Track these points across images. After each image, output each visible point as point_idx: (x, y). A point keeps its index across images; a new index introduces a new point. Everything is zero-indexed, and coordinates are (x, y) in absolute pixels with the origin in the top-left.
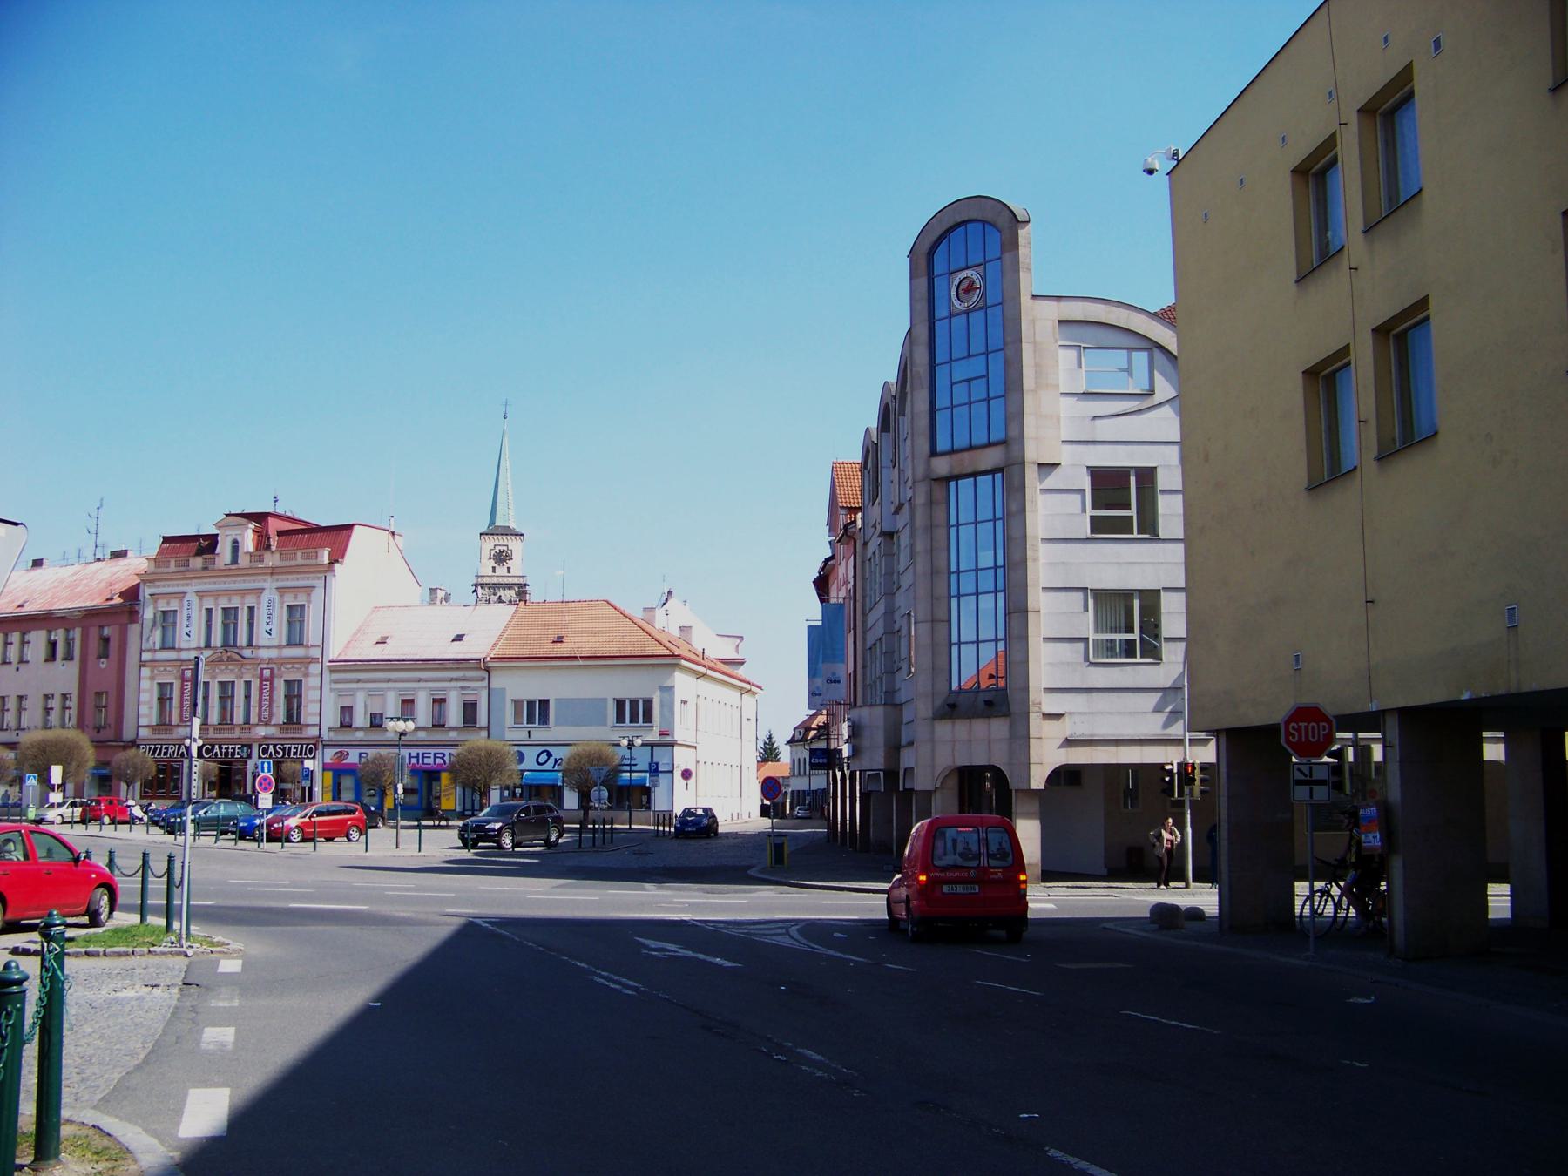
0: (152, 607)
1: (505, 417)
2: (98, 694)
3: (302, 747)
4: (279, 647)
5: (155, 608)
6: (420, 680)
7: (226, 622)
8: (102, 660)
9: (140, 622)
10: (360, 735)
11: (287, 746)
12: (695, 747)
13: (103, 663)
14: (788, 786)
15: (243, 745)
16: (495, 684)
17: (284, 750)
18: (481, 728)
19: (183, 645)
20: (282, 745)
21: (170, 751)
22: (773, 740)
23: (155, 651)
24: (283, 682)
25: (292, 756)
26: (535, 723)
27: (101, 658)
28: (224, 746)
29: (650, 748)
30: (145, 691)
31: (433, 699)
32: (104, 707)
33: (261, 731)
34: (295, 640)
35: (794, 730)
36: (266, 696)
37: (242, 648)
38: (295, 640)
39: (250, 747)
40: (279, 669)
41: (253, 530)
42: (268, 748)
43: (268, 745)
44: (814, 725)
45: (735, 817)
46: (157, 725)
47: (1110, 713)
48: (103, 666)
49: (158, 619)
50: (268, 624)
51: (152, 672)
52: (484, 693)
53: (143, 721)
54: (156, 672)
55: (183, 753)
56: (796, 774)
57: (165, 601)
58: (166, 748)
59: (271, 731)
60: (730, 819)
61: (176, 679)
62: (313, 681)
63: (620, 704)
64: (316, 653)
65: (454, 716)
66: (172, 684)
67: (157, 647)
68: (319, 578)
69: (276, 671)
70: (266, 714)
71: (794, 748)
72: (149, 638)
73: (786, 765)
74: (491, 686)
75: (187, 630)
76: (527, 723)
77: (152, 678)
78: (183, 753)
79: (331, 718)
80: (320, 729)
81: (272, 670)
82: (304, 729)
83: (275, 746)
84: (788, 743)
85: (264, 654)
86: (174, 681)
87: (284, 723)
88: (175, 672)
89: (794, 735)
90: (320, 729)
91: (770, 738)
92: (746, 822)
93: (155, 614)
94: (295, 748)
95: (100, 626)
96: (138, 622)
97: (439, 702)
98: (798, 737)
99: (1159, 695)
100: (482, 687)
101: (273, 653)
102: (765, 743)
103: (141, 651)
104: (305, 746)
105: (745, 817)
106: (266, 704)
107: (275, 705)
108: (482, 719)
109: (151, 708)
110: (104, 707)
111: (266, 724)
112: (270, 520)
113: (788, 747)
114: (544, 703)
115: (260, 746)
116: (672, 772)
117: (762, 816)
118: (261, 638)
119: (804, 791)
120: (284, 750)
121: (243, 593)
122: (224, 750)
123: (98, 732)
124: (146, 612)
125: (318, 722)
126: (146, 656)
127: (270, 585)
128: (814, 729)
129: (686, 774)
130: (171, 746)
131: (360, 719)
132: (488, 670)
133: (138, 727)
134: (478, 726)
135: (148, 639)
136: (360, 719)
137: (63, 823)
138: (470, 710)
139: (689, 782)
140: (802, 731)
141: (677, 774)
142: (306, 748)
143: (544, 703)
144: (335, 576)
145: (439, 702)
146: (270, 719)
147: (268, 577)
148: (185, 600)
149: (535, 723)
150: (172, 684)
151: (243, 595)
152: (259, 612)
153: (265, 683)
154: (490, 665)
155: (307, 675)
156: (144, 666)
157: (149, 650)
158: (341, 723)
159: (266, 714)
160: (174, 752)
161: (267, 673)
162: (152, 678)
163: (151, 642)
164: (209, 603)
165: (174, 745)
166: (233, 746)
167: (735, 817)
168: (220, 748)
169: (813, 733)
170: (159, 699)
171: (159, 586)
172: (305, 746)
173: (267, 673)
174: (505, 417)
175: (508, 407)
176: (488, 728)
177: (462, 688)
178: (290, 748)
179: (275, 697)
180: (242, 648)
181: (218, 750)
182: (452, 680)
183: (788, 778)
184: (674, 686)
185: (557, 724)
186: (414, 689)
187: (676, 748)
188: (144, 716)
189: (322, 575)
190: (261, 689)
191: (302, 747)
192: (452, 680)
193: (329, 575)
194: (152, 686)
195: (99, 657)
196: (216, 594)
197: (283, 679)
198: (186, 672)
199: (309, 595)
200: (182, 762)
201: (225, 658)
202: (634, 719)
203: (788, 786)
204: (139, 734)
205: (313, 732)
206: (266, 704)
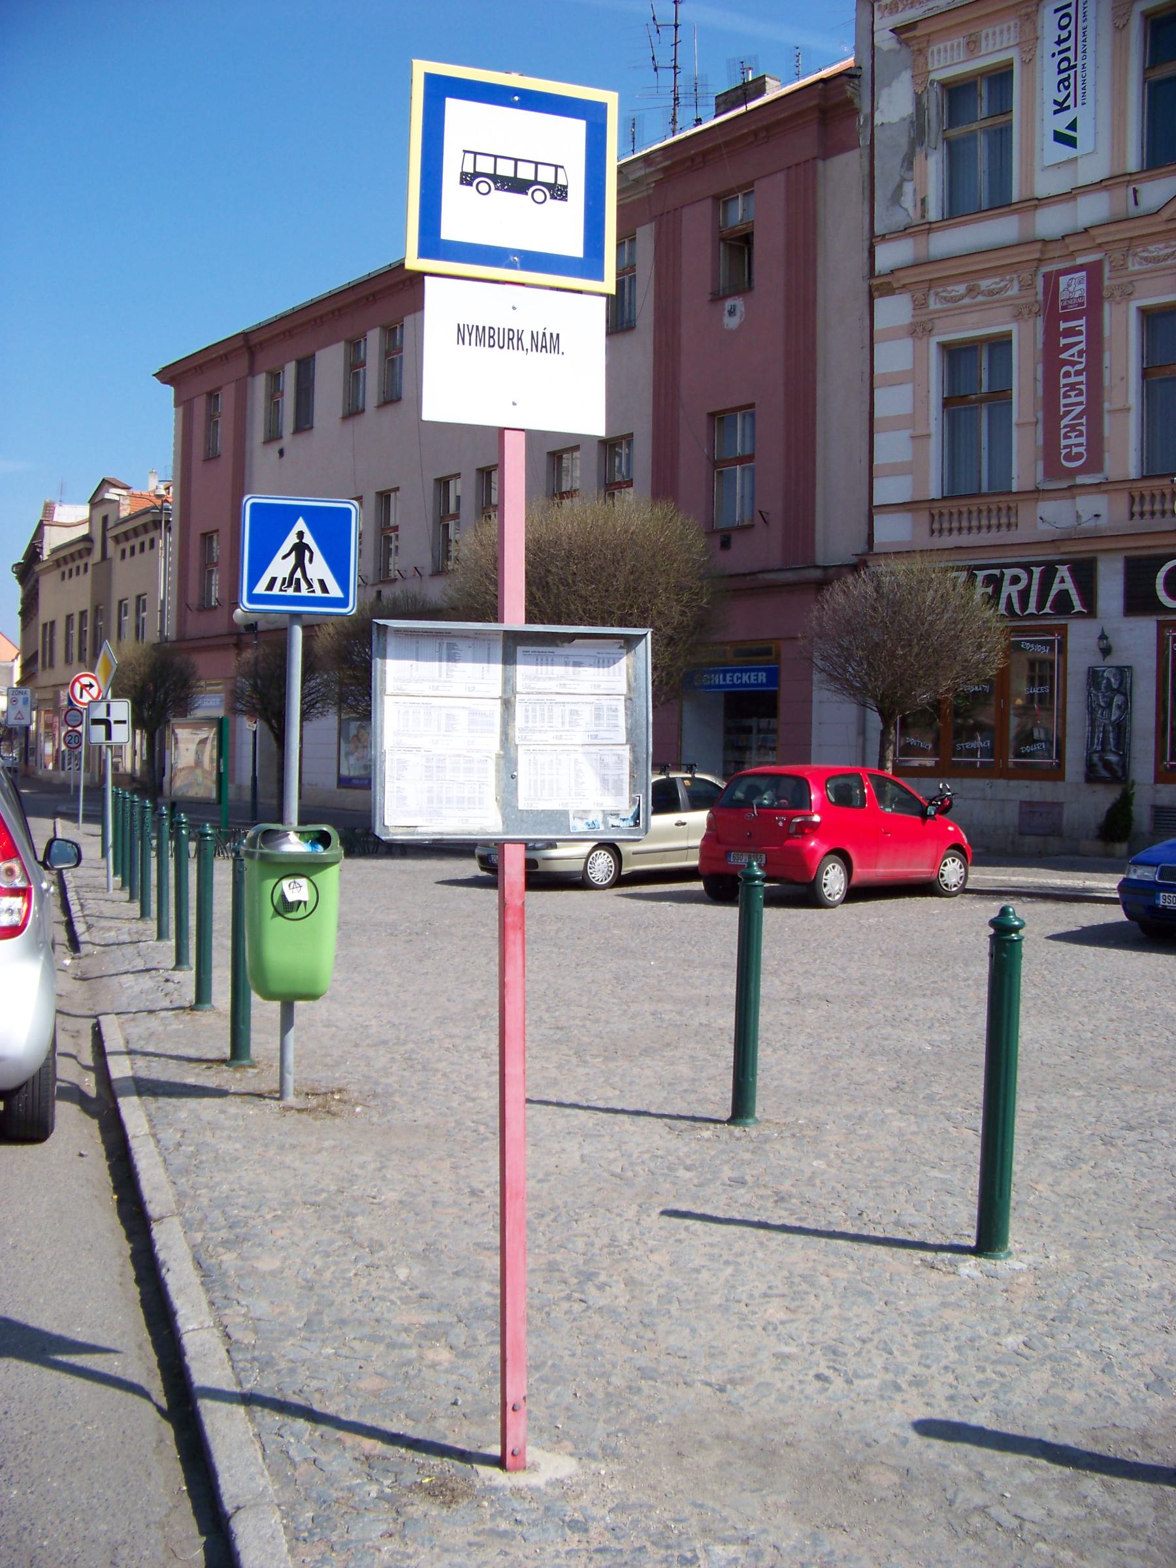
0: (906, 76)
2: (719, 419)
5: (920, 75)
7: (954, 133)
8: (728, 303)
9: (864, 141)
13: (732, 313)
19: (1044, 186)
23: (928, 228)
24: (934, 350)
27: (725, 297)
30: (895, 380)
32: (741, 460)
35: (76, 845)
36: (1073, 377)
46: (944, 498)
48: (732, 323)
49: (933, 112)
50: (1061, 107)
51: (919, 305)
53: (887, 491)
54: (934, 304)
55: (1064, 594)
57: (959, 40)
58: (989, 580)
61: (1017, 317)
66: (1000, 344)
67: (933, 214)
69: (1108, 280)
70: (1076, 443)
72: (900, 187)
75: (1061, 123)
77: (919, 330)
78: (1064, 594)
88: (1014, 290)
93: (918, 100)
95: (716, 198)
96: (853, 146)
99: (30, 820)
103: (873, 240)
106: (1073, 403)
109: (919, 439)
110: (741, 460)
123: (726, 544)
124: (882, 102)
126: (889, 256)
130: (1009, 573)
133: (872, 511)
135: (896, 196)
137: (621, 880)
150: (1000, 344)
156: (888, 290)
157: (906, 231)
159: (1076, 443)
160: (1024, 595)
161: (1073, 287)
162: (919, 330)
163: (908, 201)
165: (1027, 567)
170: (947, 403)
173: (1073, 287)
188: (896, 470)
195: (717, 297)
197: (1134, 305)
198: (1063, 281)
200: (1063, 629)
204: (877, 539)
206: (1073, 403)
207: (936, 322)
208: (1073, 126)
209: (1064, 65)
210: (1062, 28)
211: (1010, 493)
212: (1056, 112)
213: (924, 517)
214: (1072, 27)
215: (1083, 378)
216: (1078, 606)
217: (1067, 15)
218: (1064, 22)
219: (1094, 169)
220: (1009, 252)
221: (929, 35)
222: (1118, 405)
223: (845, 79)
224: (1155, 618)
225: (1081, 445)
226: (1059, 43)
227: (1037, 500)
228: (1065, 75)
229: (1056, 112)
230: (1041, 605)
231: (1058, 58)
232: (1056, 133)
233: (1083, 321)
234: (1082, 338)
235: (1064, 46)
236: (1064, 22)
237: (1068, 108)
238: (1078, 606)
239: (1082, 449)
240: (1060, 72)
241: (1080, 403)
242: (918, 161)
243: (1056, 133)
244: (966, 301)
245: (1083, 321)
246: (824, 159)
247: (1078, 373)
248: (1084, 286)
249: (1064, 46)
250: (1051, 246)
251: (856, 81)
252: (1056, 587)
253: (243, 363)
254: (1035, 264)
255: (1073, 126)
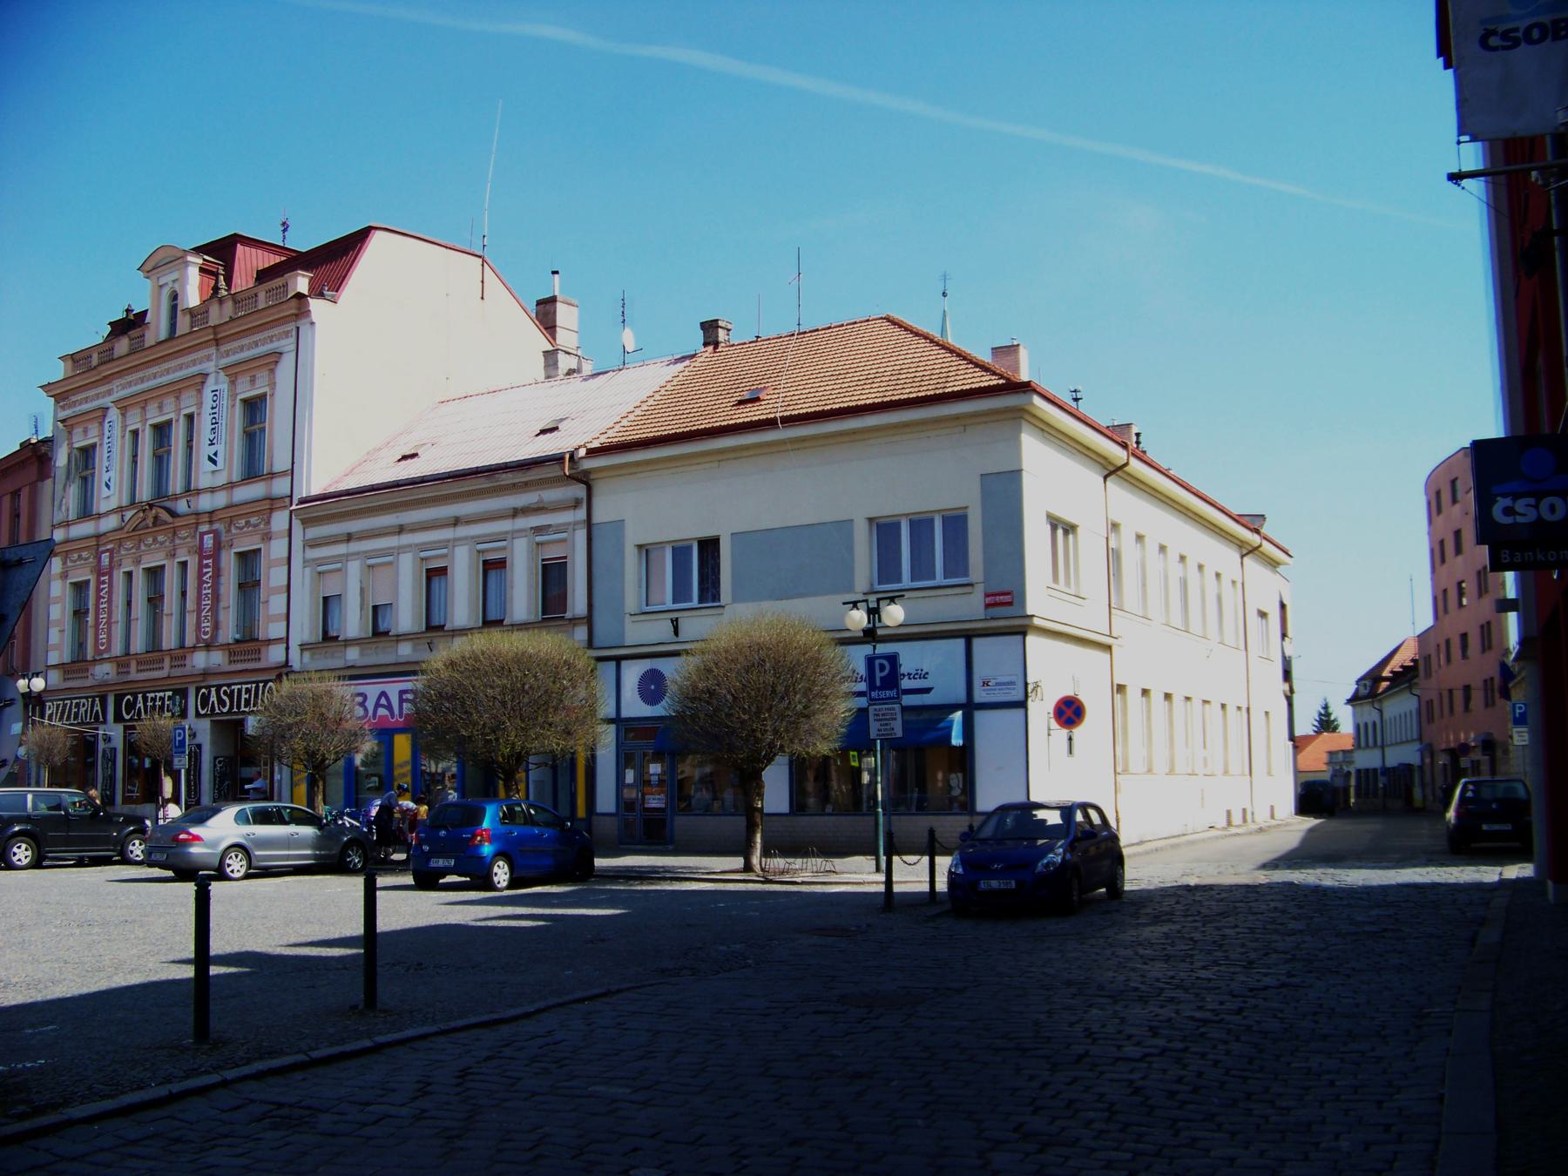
1: (944, 294)
3: (257, 688)
4: (231, 486)
5: (70, 444)
6: (456, 522)
7: (84, 474)
10: (353, 655)
11: (236, 688)
12: (1108, 648)
14: (1351, 762)
15: (176, 692)
16: (604, 511)
17: (231, 696)
18: (574, 621)
20: (229, 685)
21: (82, 710)
22: (1330, 710)
25: (243, 709)
26: (690, 600)
28: (150, 695)
29: (961, 643)
31: (485, 562)
33: (200, 660)
34: (253, 470)
37: (176, 498)
38: (253, 470)
39: (183, 693)
40: (229, 531)
41: (202, 270)
42: (210, 692)
43: (208, 687)
44: (1386, 673)
45: (1237, 819)
46: (73, 662)
47: (1155, 840)
52: (581, 536)
55: (97, 711)
56: (1363, 744)
59: (217, 659)
60: (1224, 824)
62: (278, 548)
63: (885, 531)
64: (280, 487)
65: (522, 598)
68: (287, 334)
69: (224, 538)
71: (1358, 709)
72: (62, 501)
73: (1348, 735)
74: (596, 519)
76: (675, 601)
79: (304, 627)
80: (287, 649)
81: (216, 534)
82: (263, 650)
83: (219, 687)
84: (1349, 701)
85: (205, 503)
86: (261, 546)
87: (237, 641)
89: (1357, 690)
90: (287, 649)
91: (1326, 707)
92: (1261, 830)
94: (248, 691)
96: (49, 477)
97: (493, 567)
98: (1363, 692)
100: (576, 523)
101: (221, 500)
102: (1320, 714)
104: (261, 685)
105: (1262, 818)
107: (222, 604)
108: (577, 603)
111: (208, 647)
112: (240, 249)
113: (1349, 708)
114: (710, 547)
115: (198, 690)
116: (1022, 704)
117: (1296, 814)
118: (203, 479)
119: (1375, 770)
120: (231, 696)
121: (176, 389)
122: (149, 704)
125: (283, 634)
127: (211, 363)
128: (1386, 679)
129: (1069, 712)
131: (353, 623)
132: (584, 479)
134: (568, 615)
136: (353, 623)
138: (553, 576)
139: (1078, 732)
140: (1368, 683)
141: (1041, 711)
142: (264, 687)
143: (710, 547)
144: (312, 323)
145: (493, 567)
146: (214, 636)
147: (213, 350)
148: (107, 421)
149: (690, 600)
151: (178, 394)
152: (199, 422)
153: (205, 562)
154: (588, 464)
155: (268, 537)
158: (325, 632)
160: (86, 711)
161: (209, 541)
162: (64, 576)
164: (134, 422)
165: (87, 698)
166: (162, 694)
167: (1237, 819)
168: (145, 699)
169: (1385, 684)
171: (74, 404)
172: (261, 685)
174: (944, 294)
175: (947, 281)
176: (589, 620)
177: (538, 530)
178: (240, 691)
179: (223, 590)
180: (176, 498)
181: (141, 705)
182: (516, 513)
183: (1351, 751)
184: (1020, 471)
185: (736, 599)
186: (445, 544)
187: (1031, 639)
188: (56, 647)
189: (291, 327)
190: (200, 574)
191: (257, 688)
192: (516, 513)
193: (303, 324)
194: (64, 590)
196: (141, 401)
199: (272, 371)
201: (150, 521)
202: (922, 567)
203: (1351, 762)
205: (275, 655)
207: (69, 572)
208: (215, 454)
209: (214, 421)
210: (214, 401)
211: (162, 651)
212: (210, 445)
213: (115, 665)
214: (217, 402)
215: (210, 591)
216: (101, 719)
217: (216, 395)
218: (215, 398)
219: (221, 479)
220: (259, 503)
221: (72, 425)
222: (226, 605)
223: (41, 444)
224: (122, 724)
225: (207, 627)
226: (213, 408)
227: (95, 665)
228: (213, 426)
229: (210, 445)
230: (90, 719)
231: (212, 416)
232: (209, 456)
233: (211, 561)
234: (210, 569)
235: (214, 411)
236: (215, 398)
237: (214, 444)
238: (101, 719)
239: (104, 640)
240: (212, 424)
241: (208, 605)
242: (67, 490)
243: (209, 456)
244: (78, 563)
245: (211, 561)
246: (43, 481)
247: (209, 589)
248: (212, 542)
249: (214, 411)
250: (201, 516)
251: (50, 443)
252: (95, 709)
253: (33, 469)
254: (194, 526)
255: (215, 454)
